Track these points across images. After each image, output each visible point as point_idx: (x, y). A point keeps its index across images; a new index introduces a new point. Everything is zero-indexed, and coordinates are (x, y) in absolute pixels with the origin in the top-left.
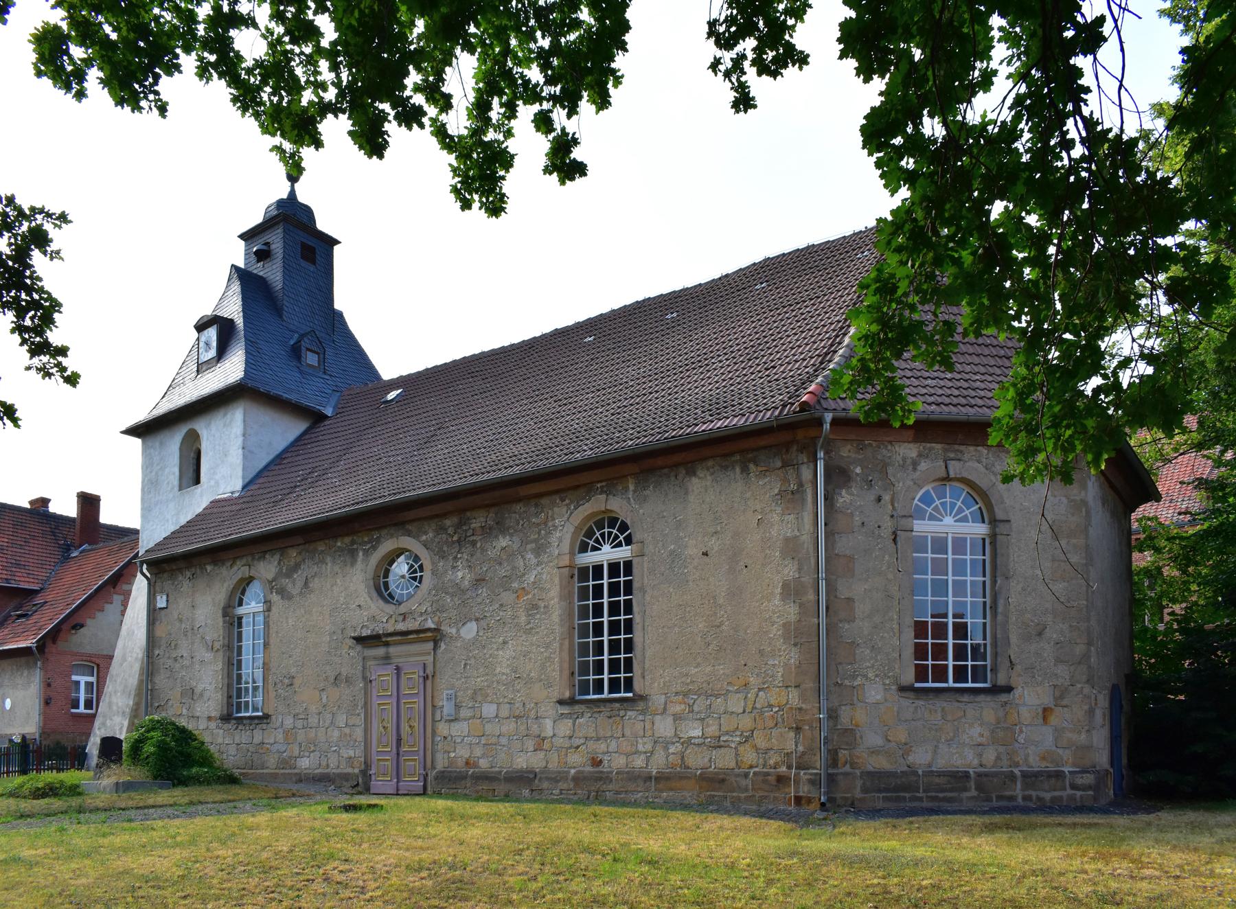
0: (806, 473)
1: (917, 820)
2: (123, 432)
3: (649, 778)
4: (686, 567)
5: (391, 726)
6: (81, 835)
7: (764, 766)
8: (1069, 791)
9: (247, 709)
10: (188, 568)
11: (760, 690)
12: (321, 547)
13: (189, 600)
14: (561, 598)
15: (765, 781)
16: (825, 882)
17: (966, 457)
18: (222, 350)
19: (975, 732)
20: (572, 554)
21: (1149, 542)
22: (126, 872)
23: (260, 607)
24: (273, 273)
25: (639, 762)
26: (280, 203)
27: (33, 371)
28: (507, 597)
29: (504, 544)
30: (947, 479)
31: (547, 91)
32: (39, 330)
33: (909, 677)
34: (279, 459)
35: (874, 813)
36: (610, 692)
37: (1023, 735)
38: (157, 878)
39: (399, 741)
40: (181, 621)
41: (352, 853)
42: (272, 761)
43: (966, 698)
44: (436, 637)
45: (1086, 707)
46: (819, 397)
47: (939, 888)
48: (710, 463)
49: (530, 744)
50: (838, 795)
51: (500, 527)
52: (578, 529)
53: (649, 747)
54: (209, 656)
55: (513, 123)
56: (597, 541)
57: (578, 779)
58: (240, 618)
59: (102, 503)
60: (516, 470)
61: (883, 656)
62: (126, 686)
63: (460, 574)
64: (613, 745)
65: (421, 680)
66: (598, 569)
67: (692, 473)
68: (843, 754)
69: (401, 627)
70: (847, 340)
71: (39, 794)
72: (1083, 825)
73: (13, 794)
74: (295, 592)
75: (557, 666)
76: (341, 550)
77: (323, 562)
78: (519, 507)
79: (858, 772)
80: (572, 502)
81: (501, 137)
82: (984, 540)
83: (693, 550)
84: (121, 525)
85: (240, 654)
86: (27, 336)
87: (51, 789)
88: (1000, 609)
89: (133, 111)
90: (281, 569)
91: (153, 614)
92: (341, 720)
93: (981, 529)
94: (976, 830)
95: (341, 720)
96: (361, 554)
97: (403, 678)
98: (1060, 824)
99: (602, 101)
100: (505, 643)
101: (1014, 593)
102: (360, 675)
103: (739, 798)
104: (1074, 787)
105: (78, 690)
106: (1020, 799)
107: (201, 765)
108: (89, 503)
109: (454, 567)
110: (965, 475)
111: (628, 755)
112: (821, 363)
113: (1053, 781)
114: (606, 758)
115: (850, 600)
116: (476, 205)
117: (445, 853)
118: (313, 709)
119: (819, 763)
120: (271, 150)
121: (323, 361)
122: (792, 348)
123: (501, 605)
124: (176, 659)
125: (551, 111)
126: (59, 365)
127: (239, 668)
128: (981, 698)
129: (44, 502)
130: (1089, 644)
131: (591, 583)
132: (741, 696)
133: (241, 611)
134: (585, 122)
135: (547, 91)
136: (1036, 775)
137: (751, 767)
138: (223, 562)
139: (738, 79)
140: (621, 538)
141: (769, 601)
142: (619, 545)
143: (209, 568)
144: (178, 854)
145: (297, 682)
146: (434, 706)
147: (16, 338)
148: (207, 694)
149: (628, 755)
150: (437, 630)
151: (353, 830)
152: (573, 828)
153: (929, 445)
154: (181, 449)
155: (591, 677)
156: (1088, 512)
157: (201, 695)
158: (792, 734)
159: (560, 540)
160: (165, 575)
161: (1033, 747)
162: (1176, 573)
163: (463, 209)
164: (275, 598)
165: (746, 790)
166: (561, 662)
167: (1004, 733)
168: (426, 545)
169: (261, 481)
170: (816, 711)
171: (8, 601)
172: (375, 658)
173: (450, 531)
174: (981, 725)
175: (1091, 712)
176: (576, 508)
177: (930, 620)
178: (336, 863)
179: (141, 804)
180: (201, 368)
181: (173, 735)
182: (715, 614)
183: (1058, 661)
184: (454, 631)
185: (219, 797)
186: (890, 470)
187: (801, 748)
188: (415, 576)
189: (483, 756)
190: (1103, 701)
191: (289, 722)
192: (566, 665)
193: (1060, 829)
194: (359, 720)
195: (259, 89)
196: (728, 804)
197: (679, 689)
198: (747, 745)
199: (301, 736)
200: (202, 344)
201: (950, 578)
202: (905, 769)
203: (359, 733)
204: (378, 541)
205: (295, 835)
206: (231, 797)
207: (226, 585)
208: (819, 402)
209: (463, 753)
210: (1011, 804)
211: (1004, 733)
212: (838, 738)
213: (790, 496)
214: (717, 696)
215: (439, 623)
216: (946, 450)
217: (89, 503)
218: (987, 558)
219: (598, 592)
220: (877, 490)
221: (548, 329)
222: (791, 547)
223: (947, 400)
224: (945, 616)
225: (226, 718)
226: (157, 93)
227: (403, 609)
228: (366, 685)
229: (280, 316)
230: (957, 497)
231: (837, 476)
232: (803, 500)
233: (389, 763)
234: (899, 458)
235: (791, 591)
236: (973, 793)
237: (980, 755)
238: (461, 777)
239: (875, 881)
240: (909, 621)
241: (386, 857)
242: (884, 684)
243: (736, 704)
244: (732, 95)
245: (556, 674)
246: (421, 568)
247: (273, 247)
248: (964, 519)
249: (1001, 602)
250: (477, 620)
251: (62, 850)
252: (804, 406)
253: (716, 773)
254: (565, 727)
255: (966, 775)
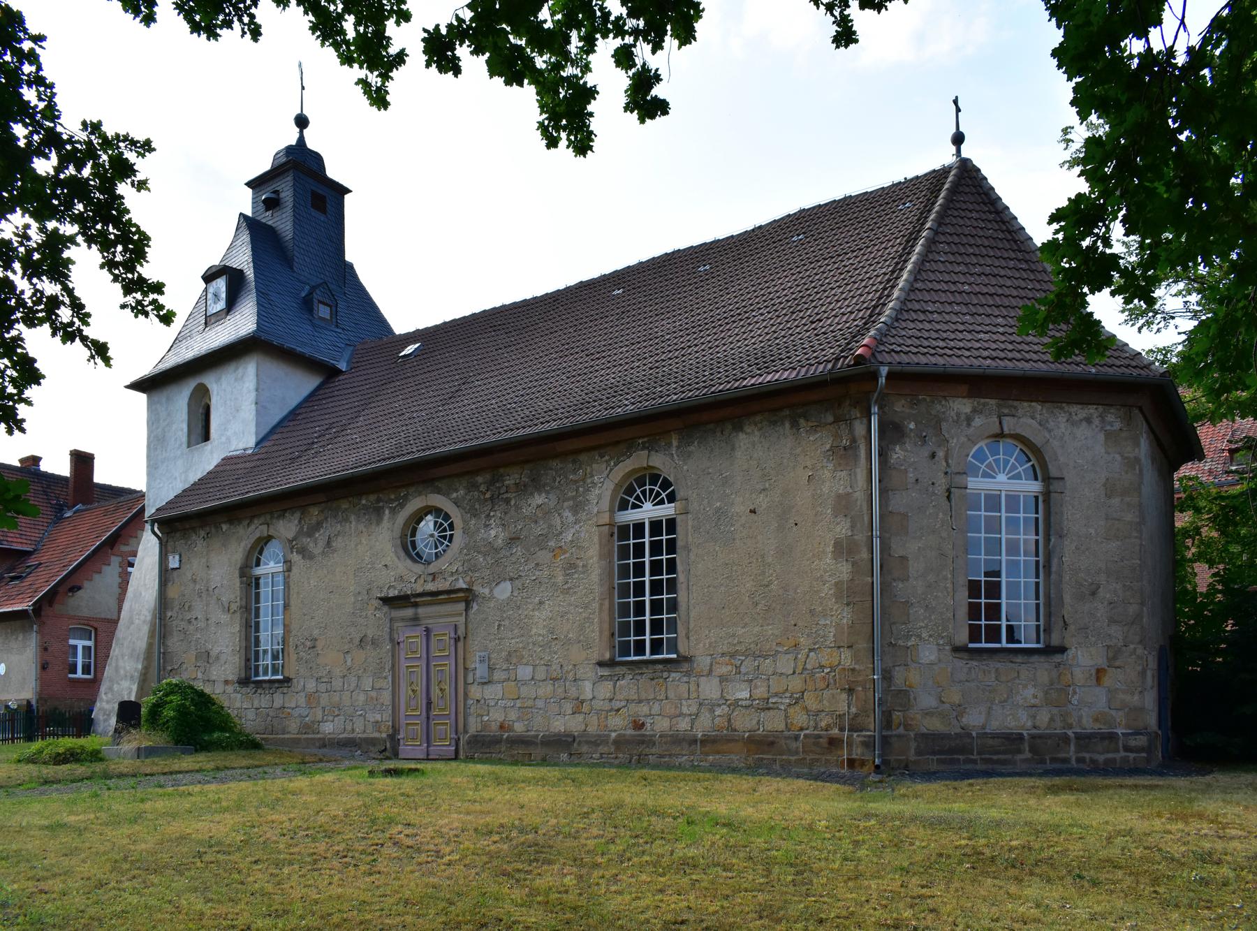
0: (859, 429)
1: (978, 783)
2: (127, 387)
3: (694, 741)
4: (732, 525)
5: (420, 687)
6: (119, 801)
7: (815, 728)
8: (1123, 754)
9: (266, 673)
10: (202, 527)
11: (811, 650)
12: (345, 505)
13: (204, 560)
14: (601, 557)
15: (816, 744)
16: (912, 844)
17: (1020, 412)
18: (232, 302)
19: (1029, 694)
20: (612, 511)
21: (1190, 503)
22: (183, 838)
23: (279, 567)
24: (283, 222)
25: (684, 725)
26: (289, 150)
27: (128, 310)
28: (544, 556)
29: (540, 502)
30: (1000, 435)
31: (631, 23)
32: (130, 266)
33: (962, 637)
34: (293, 415)
35: (930, 776)
36: (652, 653)
37: (1076, 697)
38: (219, 843)
39: (429, 704)
40: (195, 581)
41: (412, 816)
42: (293, 726)
43: (1019, 659)
44: (467, 597)
45: (1140, 668)
46: (873, 350)
47: (1030, 849)
48: (758, 418)
49: (568, 707)
50: (892, 758)
51: (536, 485)
52: (618, 486)
53: (694, 709)
54: (224, 618)
55: (591, 58)
56: (638, 498)
57: (619, 743)
58: (258, 579)
59: (96, 462)
60: (554, 425)
61: (937, 615)
62: (133, 650)
63: (493, 533)
64: (656, 708)
65: (452, 641)
66: (639, 528)
67: (739, 428)
68: (897, 716)
69: (431, 587)
70: (896, 293)
71: (60, 759)
72: (1145, 787)
73: (32, 760)
74: (317, 551)
75: (596, 627)
76: (366, 508)
77: (347, 520)
78: (555, 464)
79: (912, 734)
80: (611, 458)
81: (577, 72)
82: (1036, 498)
83: (739, 508)
84: (114, 484)
85: (257, 615)
86: (117, 272)
87: (72, 755)
88: (1054, 569)
89: (208, 39)
90: (302, 528)
91: (165, 575)
92: (367, 683)
93: (1035, 487)
94: (1039, 791)
95: (367, 683)
96: (387, 512)
97: (433, 640)
98: (1121, 786)
99: (686, 36)
100: (541, 603)
101: (1068, 552)
102: (387, 637)
103: (789, 762)
104: (1127, 749)
105: (75, 655)
106: (1073, 762)
107: (223, 730)
108: (83, 461)
109: (486, 526)
110: (1019, 431)
111: (671, 718)
112: (871, 316)
113: (1107, 742)
114: (649, 720)
115: (904, 559)
116: (563, 143)
117: (507, 817)
118: (337, 672)
119: (872, 725)
120: (357, 84)
121: (335, 313)
122: (838, 301)
123: (537, 564)
124: (189, 622)
125: (635, 46)
126: (154, 302)
127: (257, 630)
128: (1035, 658)
129: (35, 460)
130: (1142, 604)
131: (632, 542)
132: (791, 656)
133: (258, 571)
134: (670, 61)
135: (631, 23)
136: (1090, 737)
137: (802, 729)
138: (239, 521)
139: (841, 12)
140: (664, 495)
141: (820, 560)
142: (662, 502)
143: (225, 527)
144: (230, 820)
145: (320, 644)
146: (466, 669)
147: (106, 275)
148: (223, 658)
149: (671, 718)
150: (468, 590)
151: (402, 794)
152: (629, 791)
153: (982, 400)
154: (189, 405)
155: (632, 638)
156: (1141, 470)
157: (217, 658)
158: (844, 696)
159: (600, 497)
160: (178, 535)
161: (1086, 709)
162: (1215, 534)
163: (548, 147)
164: (296, 557)
165: (797, 753)
166: (601, 622)
167: (1058, 694)
168: (456, 503)
169: (275, 437)
170: (869, 671)
171: (4, 563)
172: (403, 620)
173: (483, 488)
174: (1034, 686)
175: (1143, 673)
176: (616, 465)
177: (983, 579)
178: (400, 827)
179: (166, 770)
180: (210, 320)
181: (192, 699)
182: (764, 573)
183: (1112, 621)
184: (486, 591)
185: (245, 763)
186: (944, 425)
187: (853, 710)
188: (445, 533)
189: (519, 719)
190: (1153, 664)
191: (311, 686)
192: (606, 626)
193: (1124, 791)
194: (387, 684)
195: (340, 17)
196: (777, 767)
197: (725, 649)
198: (797, 708)
199: (324, 699)
200: (210, 296)
201: (1004, 536)
202: (959, 730)
203: (386, 697)
204: (406, 498)
205: (344, 799)
206: (257, 763)
207: (243, 544)
208: (873, 354)
209: (497, 716)
210: (1065, 766)
211: (1058, 694)
212: (893, 700)
213: (842, 452)
214: (765, 657)
215: (471, 583)
216: (999, 406)
217: (83, 461)
218: (1040, 516)
219: (639, 551)
220: (931, 446)
221: (572, 281)
222: (843, 505)
223: (1002, 355)
224: (998, 574)
225: (244, 682)
226: (252, 17)
227: (432, 568)
228: (393, 647)
229: (291, 268)
230: (1010, 454)
231: (892, 432)
232: (856, 457)
233: (419, 727)
234: (953, 414)
235: (843, 549)
236: (1028, 755)
237: (1035, 717)
238: (496, 741)
239: (963, 842)
240: (962, 581)
241: (451, 821)
242: (938, 645)
243: (785, 664)
244: (833, 30)
245: (596, 635)
246: (451, 527)
247: (282, 195)
248: (1018, 477)
249: (1055, 562)
250: (511, 579)
251: (103, 816)
252: (859, 360)
253: (765, 736)
254: (605, 689)
255: (1020, 737)
